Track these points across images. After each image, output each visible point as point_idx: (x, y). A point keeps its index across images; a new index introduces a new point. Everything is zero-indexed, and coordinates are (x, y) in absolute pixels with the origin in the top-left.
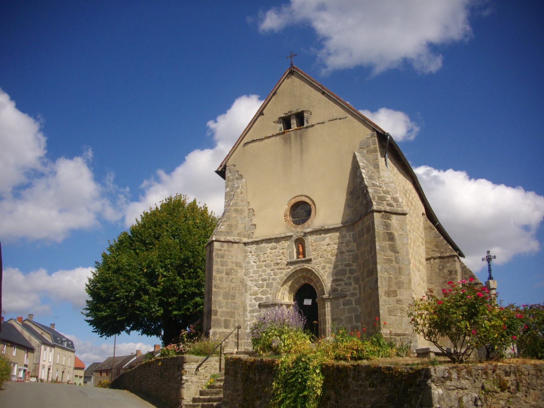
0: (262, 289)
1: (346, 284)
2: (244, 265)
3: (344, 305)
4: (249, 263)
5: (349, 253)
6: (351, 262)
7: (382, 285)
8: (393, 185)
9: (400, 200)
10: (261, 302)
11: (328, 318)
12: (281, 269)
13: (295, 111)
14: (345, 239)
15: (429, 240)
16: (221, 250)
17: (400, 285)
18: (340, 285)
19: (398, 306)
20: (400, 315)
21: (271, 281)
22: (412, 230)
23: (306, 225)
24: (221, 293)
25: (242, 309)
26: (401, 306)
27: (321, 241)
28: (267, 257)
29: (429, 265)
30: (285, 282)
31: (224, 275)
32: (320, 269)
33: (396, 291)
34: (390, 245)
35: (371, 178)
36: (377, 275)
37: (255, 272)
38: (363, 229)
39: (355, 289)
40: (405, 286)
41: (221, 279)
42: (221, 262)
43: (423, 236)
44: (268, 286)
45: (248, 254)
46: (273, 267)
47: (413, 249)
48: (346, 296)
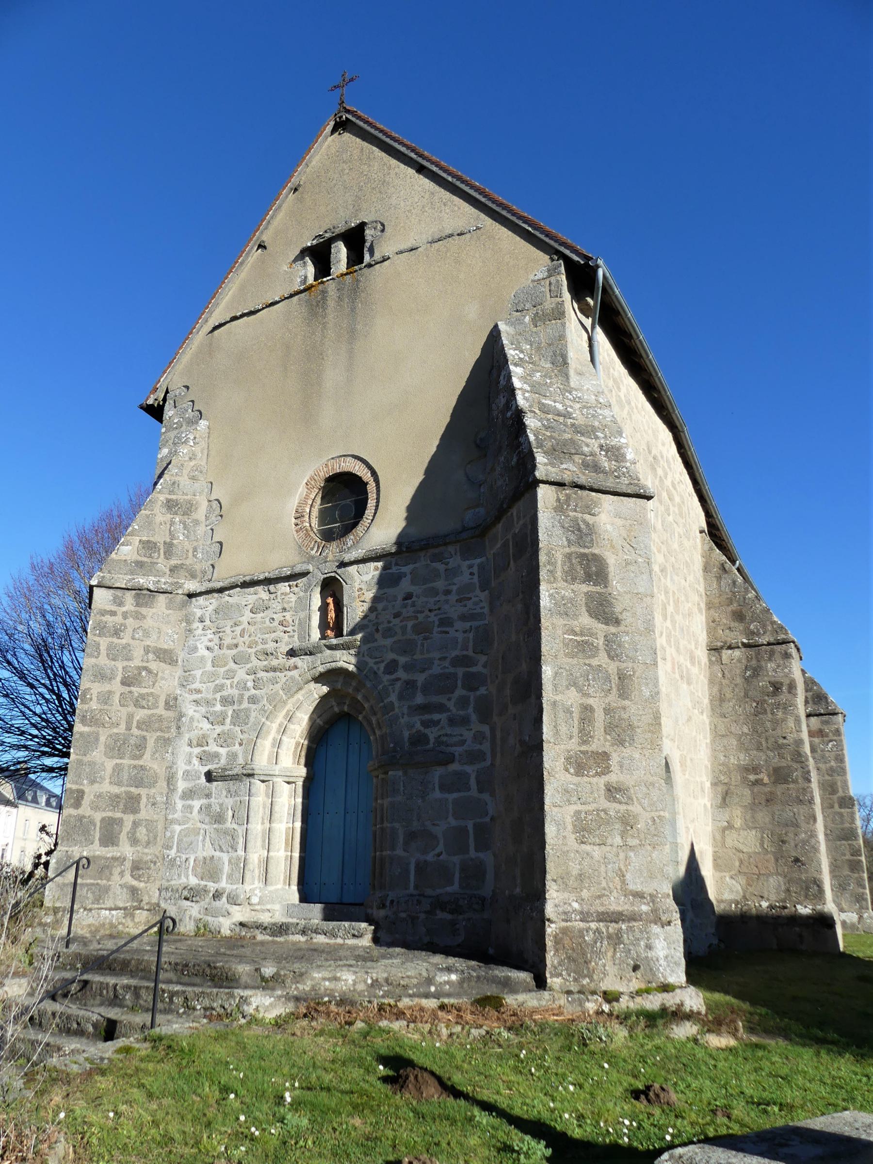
0: (219, 729)
1: (452, 722)
2: (181, 656)
4: (195, 649)
5: (467, 625)
6: (470, 653)
7: (557, 732)
8: (606, 412)
9: (630, 456)
12: (274, 670)
13: (341, 228)
14: (456, 580)
15: (717, 601)
16: (113, 613)
17: (621, 731)
18: (436, 723)
19: (613, 808)
20: (618, 840)
21: (245, 705)
22: (669, 569)
23: (350, 539)
24: (224, 877)
25: (162, 784)
26: (623, 808)
29: (717, 668)
31: (116, 686)
32: (380, 672)
33: (606, 756)
34: (589, 596)
35: (536, 389)
36: (539, 696)
37: (210, 677)
38: (505, 545)
39: (479, 737)
40: (641, 736)
41: (105, 698)
42: (110, 647)
43: (702, 589)
44: (239, 718)
46: (255, 662)
47: (673, 622)
48: (450, 759)
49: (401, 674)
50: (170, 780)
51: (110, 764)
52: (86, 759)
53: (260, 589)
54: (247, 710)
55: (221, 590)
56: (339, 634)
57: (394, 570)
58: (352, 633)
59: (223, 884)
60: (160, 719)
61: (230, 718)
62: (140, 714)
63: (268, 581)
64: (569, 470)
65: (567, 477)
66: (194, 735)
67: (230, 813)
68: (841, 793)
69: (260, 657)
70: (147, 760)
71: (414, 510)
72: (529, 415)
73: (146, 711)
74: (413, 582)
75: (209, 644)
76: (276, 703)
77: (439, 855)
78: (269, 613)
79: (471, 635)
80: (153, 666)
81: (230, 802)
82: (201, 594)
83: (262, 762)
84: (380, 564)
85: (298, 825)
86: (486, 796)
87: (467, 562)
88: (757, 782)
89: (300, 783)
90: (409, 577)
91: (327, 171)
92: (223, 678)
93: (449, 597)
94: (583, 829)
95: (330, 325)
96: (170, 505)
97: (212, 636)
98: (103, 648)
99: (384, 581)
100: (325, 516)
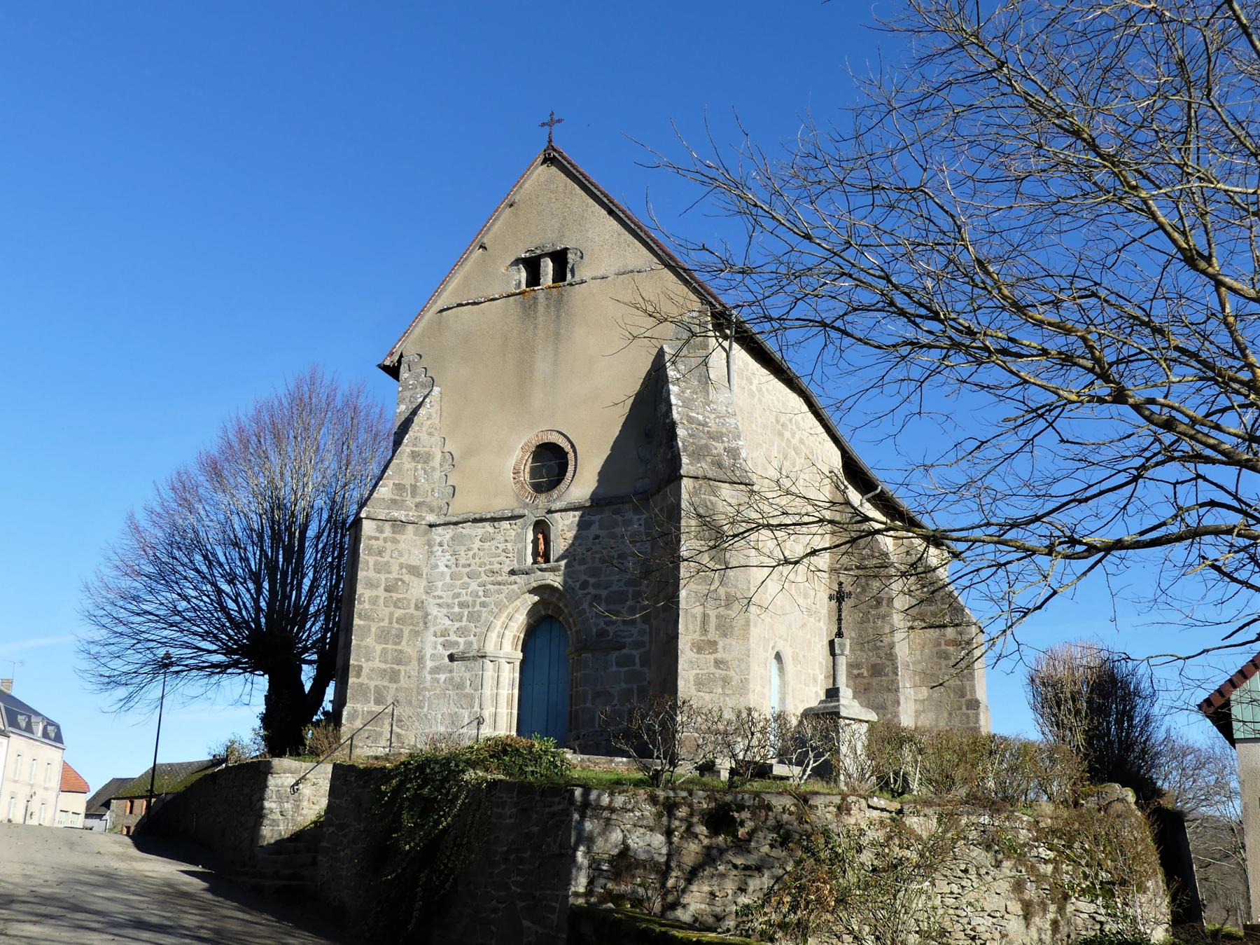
0: (457, 625)
2: (425, 571)
4: (436, 566)
7: (687, 629)
8: (732, 421)
9: (743, 455)
10: (454, 651)
11: (503, 701)
12: (499, 584)
13: (549, 249)
16: (377, 539)
19: (718, 672)
20: (720, 691)
21: (477, 608)
23: (555, 493)
25: (415, 663)
33: (715, 643)
35: (687, 404)
37: (450, 587)
39: (642, 632)
41: (374, 601)
42: (376, 564)
44: (471, 618)
46: (484, 578)
48: (623, 646)
49: (591, 590)
50: (421, 660)
51: (379, 648)
52: (363, 644)
53: (487, 524)
54: (479, 612)
55: (456, 524)
56: (547, 561)
57: (587, 518)
58: (557, 561)
60: (412, 616)
62: (399, 613)
63: (493, 520)
64: (704, 467)
65: (700, 473)
66: (438, 629)
68: (968, 697)
70: (403, 646)
71: (604, 475)
72: (680, 426)
73: (403, 611)
74: (600, 528)
76: (501, 607)
78: (494, 543)
80: (406, 578)
81: (468, 675)
82: (439, 525)
83: (490, 648)
84: (578, 513)
85: (516, 692)
86: (645, 670)
88: (859, 676)
89: (518, 664)
90: (597, 524)
91: (538, 196)
94: (700, 684)
95: (540, 326)
96: (414, 456)
98: (371, 564)
99: (583, 525)
100: (534, 472)
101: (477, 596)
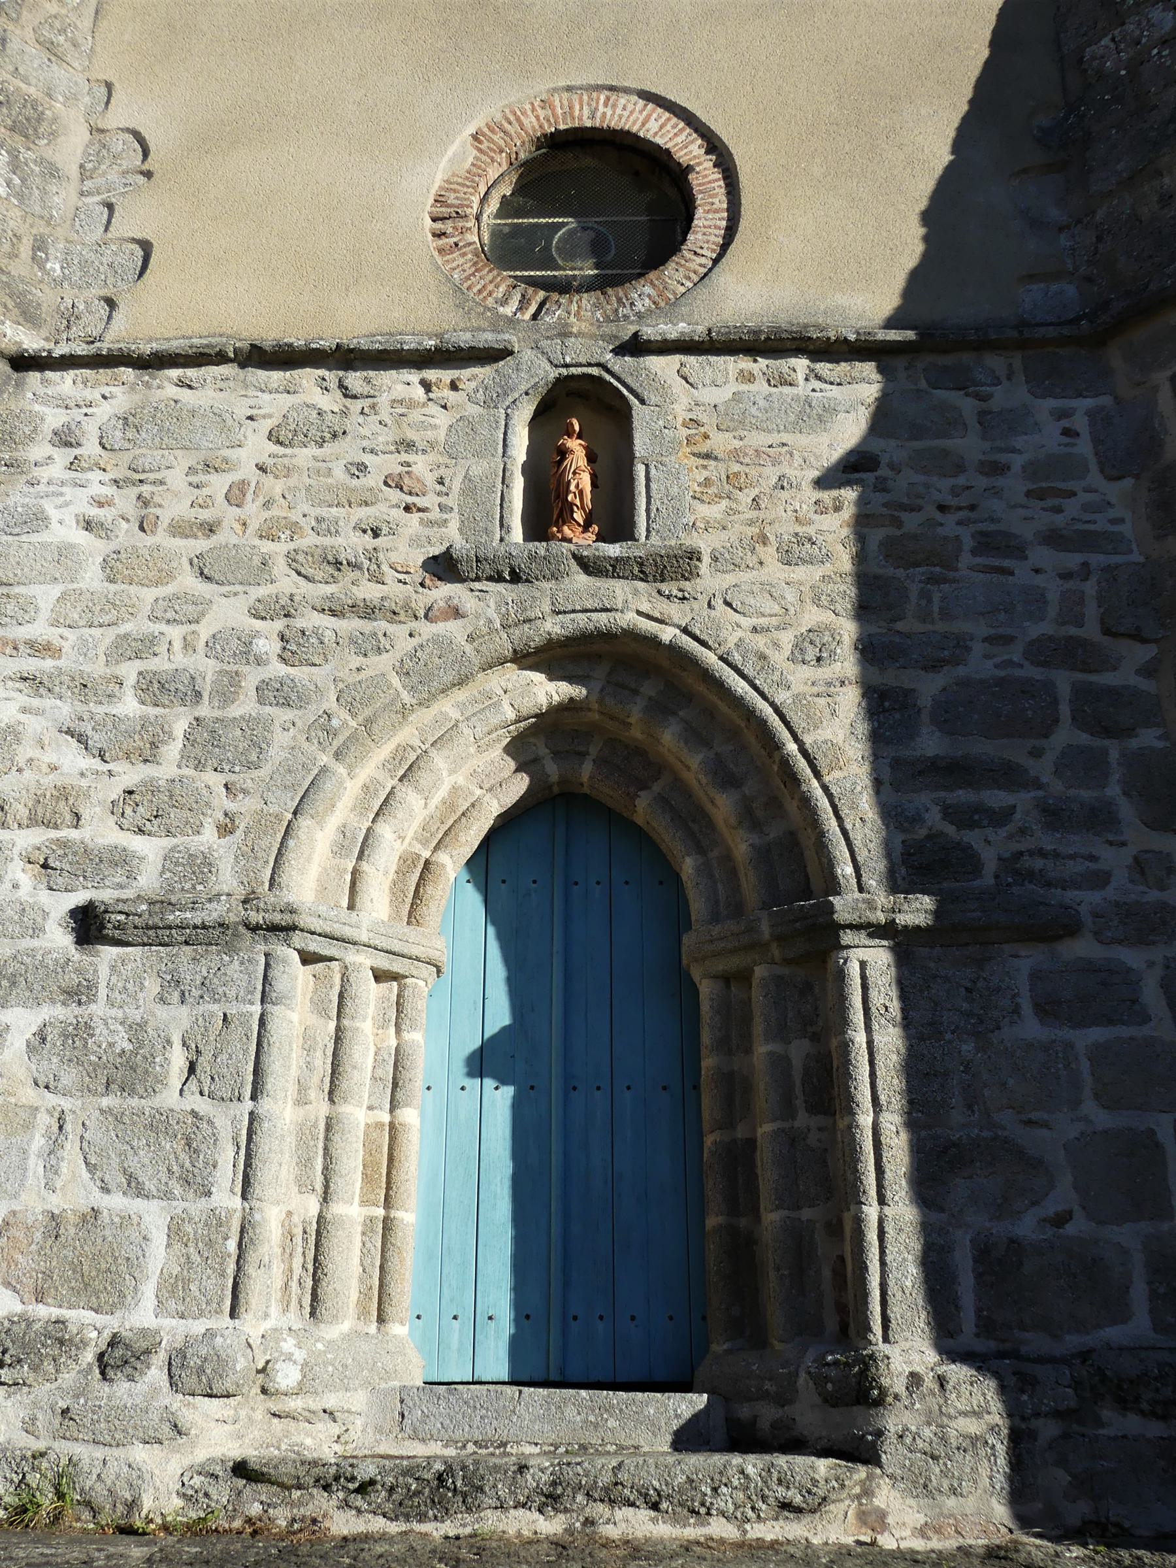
0: (130, 775)
1: (1054, 815)
3: (1046, 1009)
4: (37, 520)
5: (1073, 560)
6: (1091, 630)
10: (105, 895)
12: (368, 611)
18: (1001, 817)
21: (245, 706)
24: (149, 1290)
27: (797, 427)
28: (236, 495)
30: (549, 657)
32: (778, 658)
45: (39, 451)
46: (286, 583)
48: (1066, 926)
53: (307, 377)
59: (143, 1315)
61: (179, 744)
63: (346, 358)
67: (178, 1059)
69: (310, 572)
75: (94, 512)
76: (369, 713)
77: (1061, 1220)
78: (347, 450)
79: (1090, 588)
81: (176, 1020)
83: (308, 885)
87: (1051, 403)
92: (55, 623)
93: (999, 482)
97: (110, 490)
101: (246, 652)
